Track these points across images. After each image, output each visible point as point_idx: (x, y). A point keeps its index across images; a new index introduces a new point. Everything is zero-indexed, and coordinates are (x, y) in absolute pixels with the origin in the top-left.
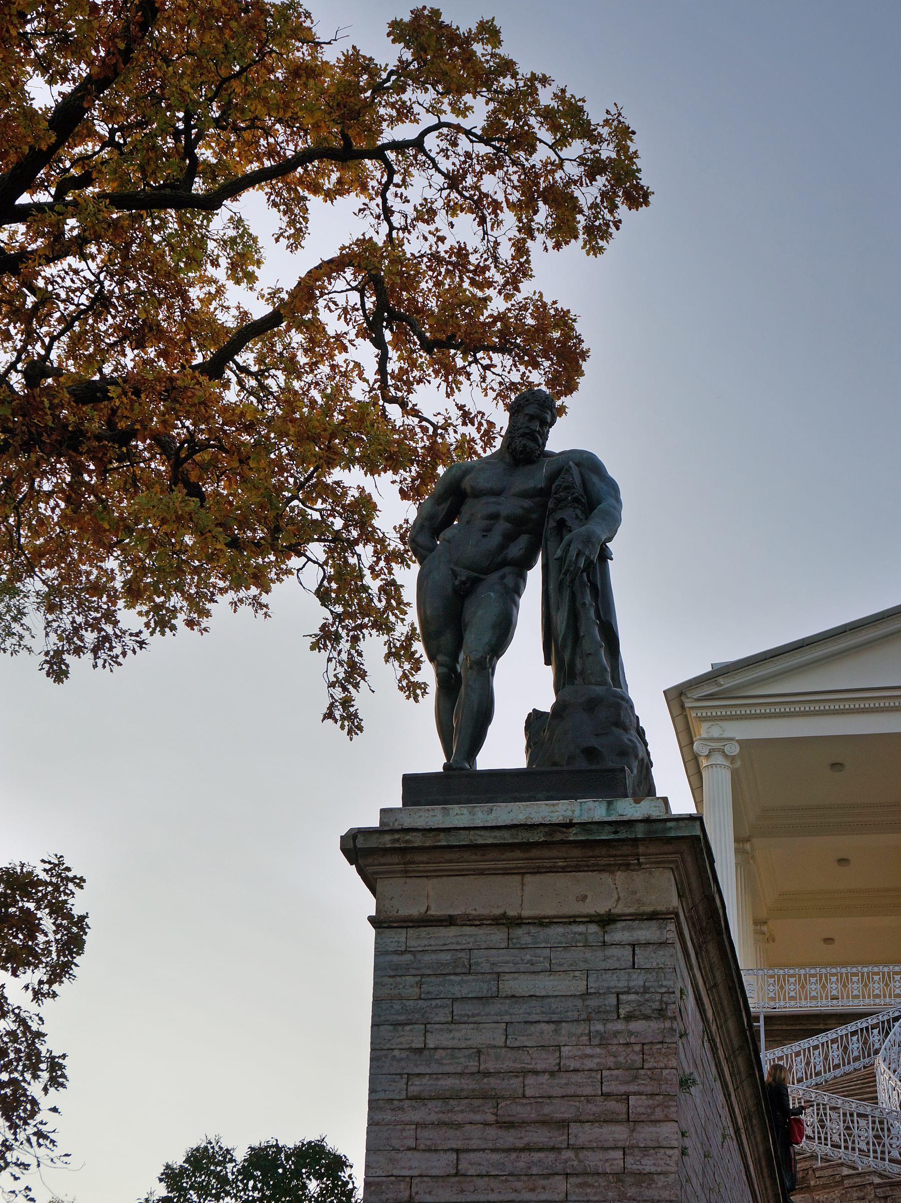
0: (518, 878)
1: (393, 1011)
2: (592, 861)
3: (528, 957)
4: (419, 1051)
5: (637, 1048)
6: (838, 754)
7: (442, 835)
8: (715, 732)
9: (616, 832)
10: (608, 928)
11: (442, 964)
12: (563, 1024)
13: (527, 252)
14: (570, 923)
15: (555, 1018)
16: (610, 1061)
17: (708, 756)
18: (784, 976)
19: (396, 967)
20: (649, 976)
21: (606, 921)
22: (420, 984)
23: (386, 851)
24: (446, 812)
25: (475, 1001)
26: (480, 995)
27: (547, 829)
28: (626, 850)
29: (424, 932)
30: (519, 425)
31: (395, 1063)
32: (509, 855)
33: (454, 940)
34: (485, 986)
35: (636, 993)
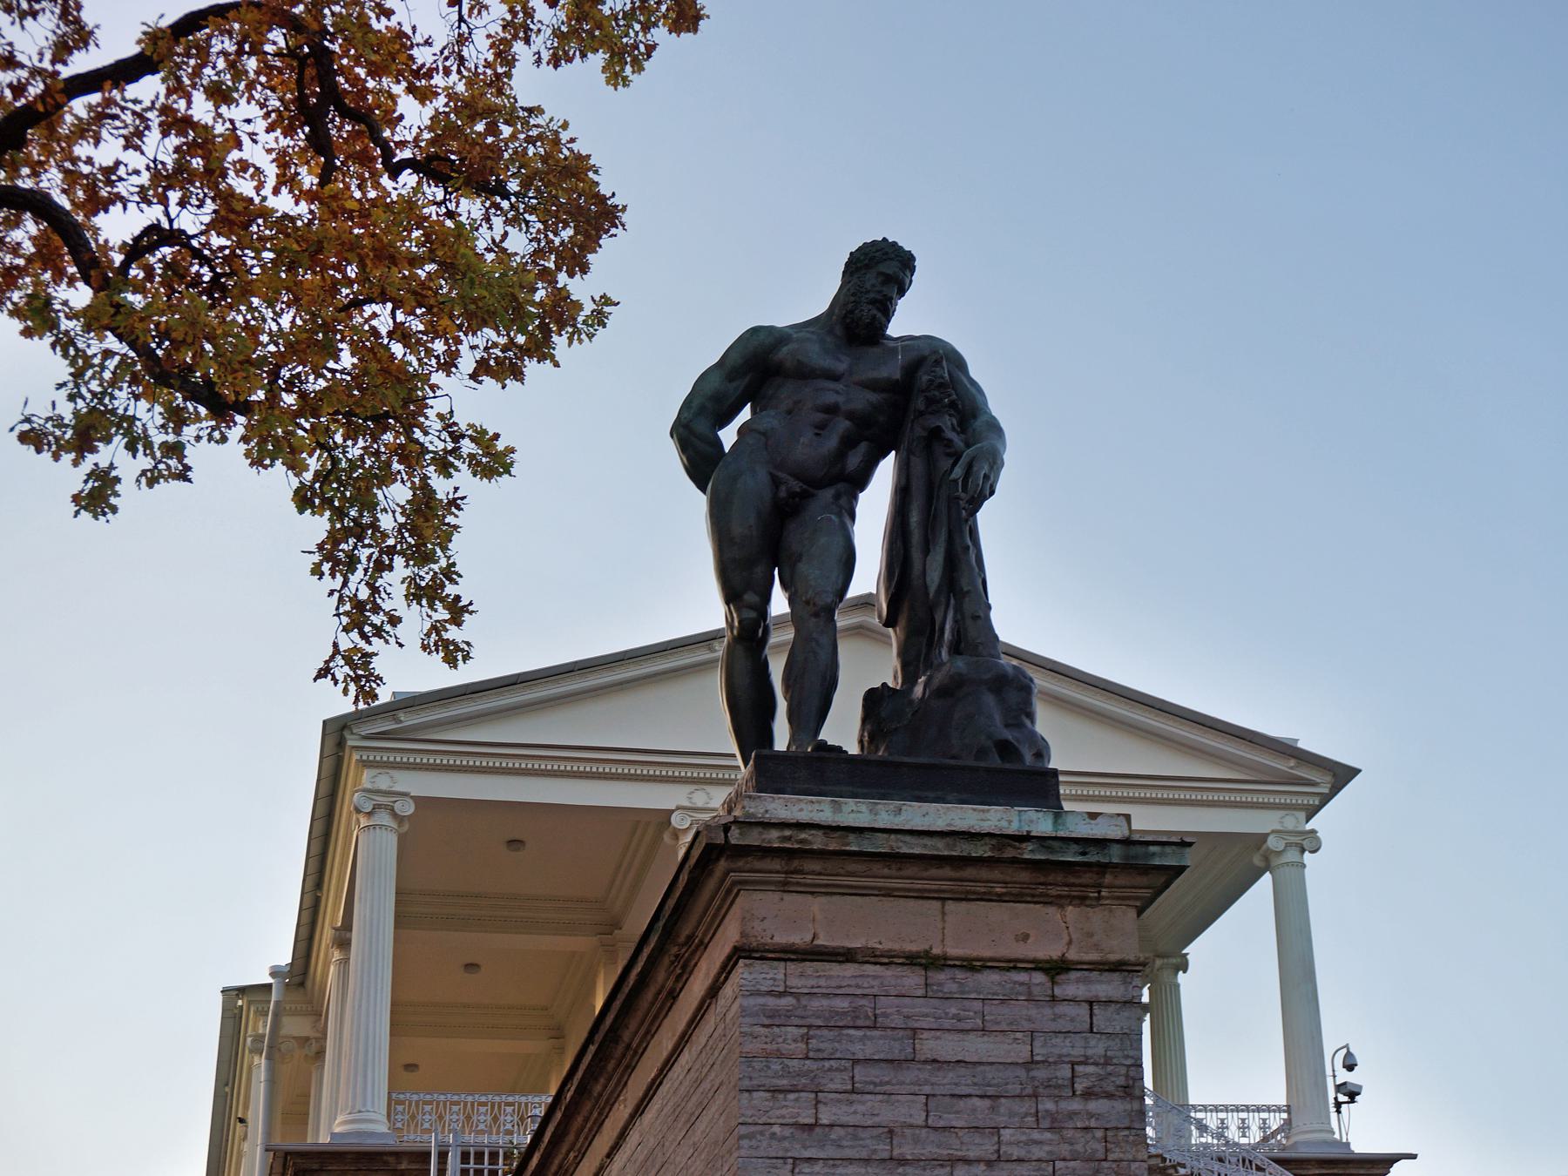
0: (937, 904)
1: (770, 1073)
2: (1041, 889)
3: (953, 1011)
4: (810, 1127)
5: (1099, 1134)
6: (518, 827)
7: (852, 837)
8: (383, 782)
9: (1084, 854)
10: (1058, 978)
11: (837, 1013)
12: (1003, 1100)
13: (511, 63)
14: (1008, 969)
15: (991, 1091)
16: (1065, 1150)
17: (369, 814)
18: (417, 1103)
19: (773, 1014)
20: (1110, 1043)
21: (1056, 969)
22: (806, 1039)
23: (766, 852)
24: (837, 808)
25: (883, 1065)
26: (890, 1057)
27: (994, 842)
28: (1087, 878)
29: (809, 967)
30: (868, 285)
31: (774, 1143)
32: (934, 872)
33: (853, 982)
34: (897, 1045)
35: (1096, 1064)
